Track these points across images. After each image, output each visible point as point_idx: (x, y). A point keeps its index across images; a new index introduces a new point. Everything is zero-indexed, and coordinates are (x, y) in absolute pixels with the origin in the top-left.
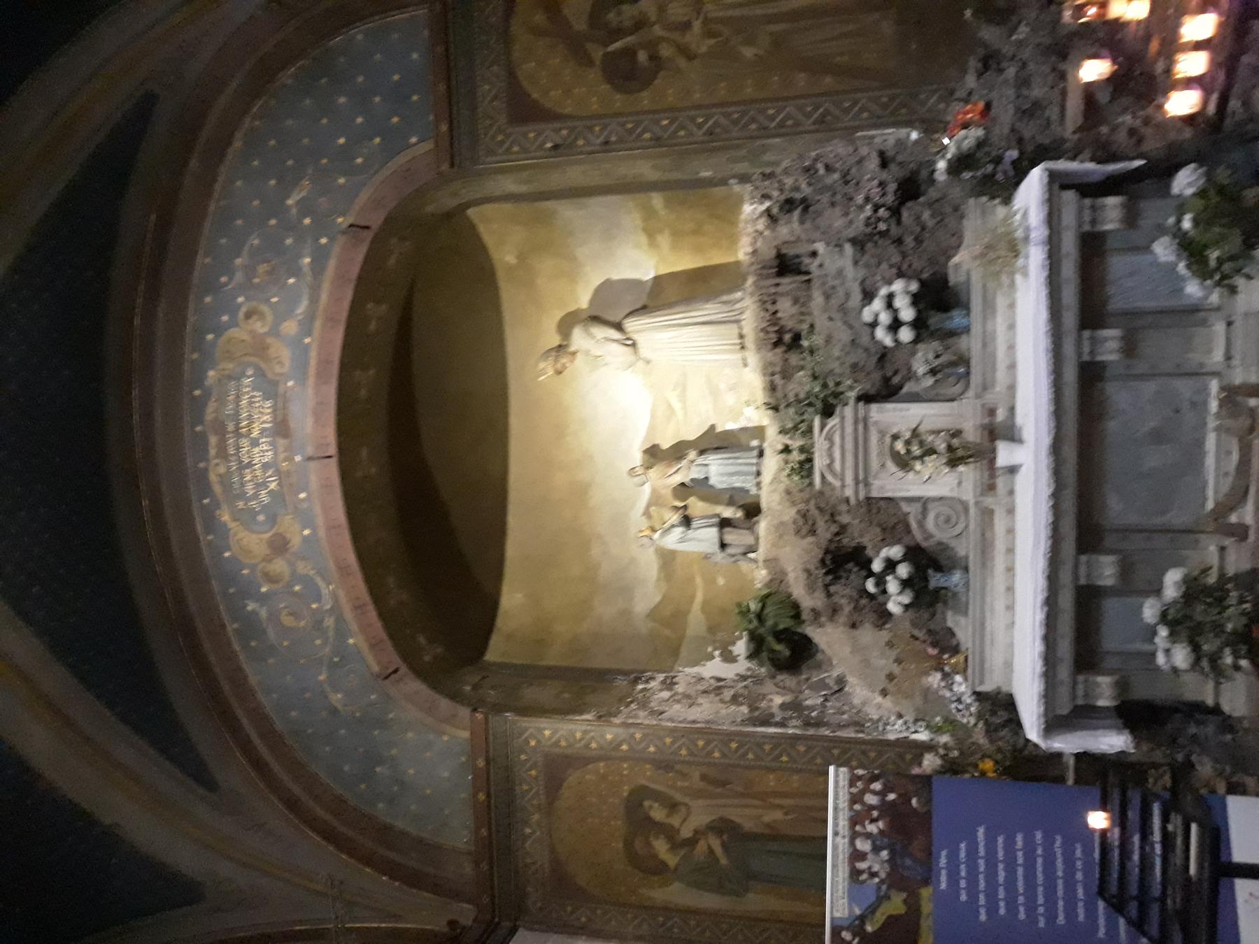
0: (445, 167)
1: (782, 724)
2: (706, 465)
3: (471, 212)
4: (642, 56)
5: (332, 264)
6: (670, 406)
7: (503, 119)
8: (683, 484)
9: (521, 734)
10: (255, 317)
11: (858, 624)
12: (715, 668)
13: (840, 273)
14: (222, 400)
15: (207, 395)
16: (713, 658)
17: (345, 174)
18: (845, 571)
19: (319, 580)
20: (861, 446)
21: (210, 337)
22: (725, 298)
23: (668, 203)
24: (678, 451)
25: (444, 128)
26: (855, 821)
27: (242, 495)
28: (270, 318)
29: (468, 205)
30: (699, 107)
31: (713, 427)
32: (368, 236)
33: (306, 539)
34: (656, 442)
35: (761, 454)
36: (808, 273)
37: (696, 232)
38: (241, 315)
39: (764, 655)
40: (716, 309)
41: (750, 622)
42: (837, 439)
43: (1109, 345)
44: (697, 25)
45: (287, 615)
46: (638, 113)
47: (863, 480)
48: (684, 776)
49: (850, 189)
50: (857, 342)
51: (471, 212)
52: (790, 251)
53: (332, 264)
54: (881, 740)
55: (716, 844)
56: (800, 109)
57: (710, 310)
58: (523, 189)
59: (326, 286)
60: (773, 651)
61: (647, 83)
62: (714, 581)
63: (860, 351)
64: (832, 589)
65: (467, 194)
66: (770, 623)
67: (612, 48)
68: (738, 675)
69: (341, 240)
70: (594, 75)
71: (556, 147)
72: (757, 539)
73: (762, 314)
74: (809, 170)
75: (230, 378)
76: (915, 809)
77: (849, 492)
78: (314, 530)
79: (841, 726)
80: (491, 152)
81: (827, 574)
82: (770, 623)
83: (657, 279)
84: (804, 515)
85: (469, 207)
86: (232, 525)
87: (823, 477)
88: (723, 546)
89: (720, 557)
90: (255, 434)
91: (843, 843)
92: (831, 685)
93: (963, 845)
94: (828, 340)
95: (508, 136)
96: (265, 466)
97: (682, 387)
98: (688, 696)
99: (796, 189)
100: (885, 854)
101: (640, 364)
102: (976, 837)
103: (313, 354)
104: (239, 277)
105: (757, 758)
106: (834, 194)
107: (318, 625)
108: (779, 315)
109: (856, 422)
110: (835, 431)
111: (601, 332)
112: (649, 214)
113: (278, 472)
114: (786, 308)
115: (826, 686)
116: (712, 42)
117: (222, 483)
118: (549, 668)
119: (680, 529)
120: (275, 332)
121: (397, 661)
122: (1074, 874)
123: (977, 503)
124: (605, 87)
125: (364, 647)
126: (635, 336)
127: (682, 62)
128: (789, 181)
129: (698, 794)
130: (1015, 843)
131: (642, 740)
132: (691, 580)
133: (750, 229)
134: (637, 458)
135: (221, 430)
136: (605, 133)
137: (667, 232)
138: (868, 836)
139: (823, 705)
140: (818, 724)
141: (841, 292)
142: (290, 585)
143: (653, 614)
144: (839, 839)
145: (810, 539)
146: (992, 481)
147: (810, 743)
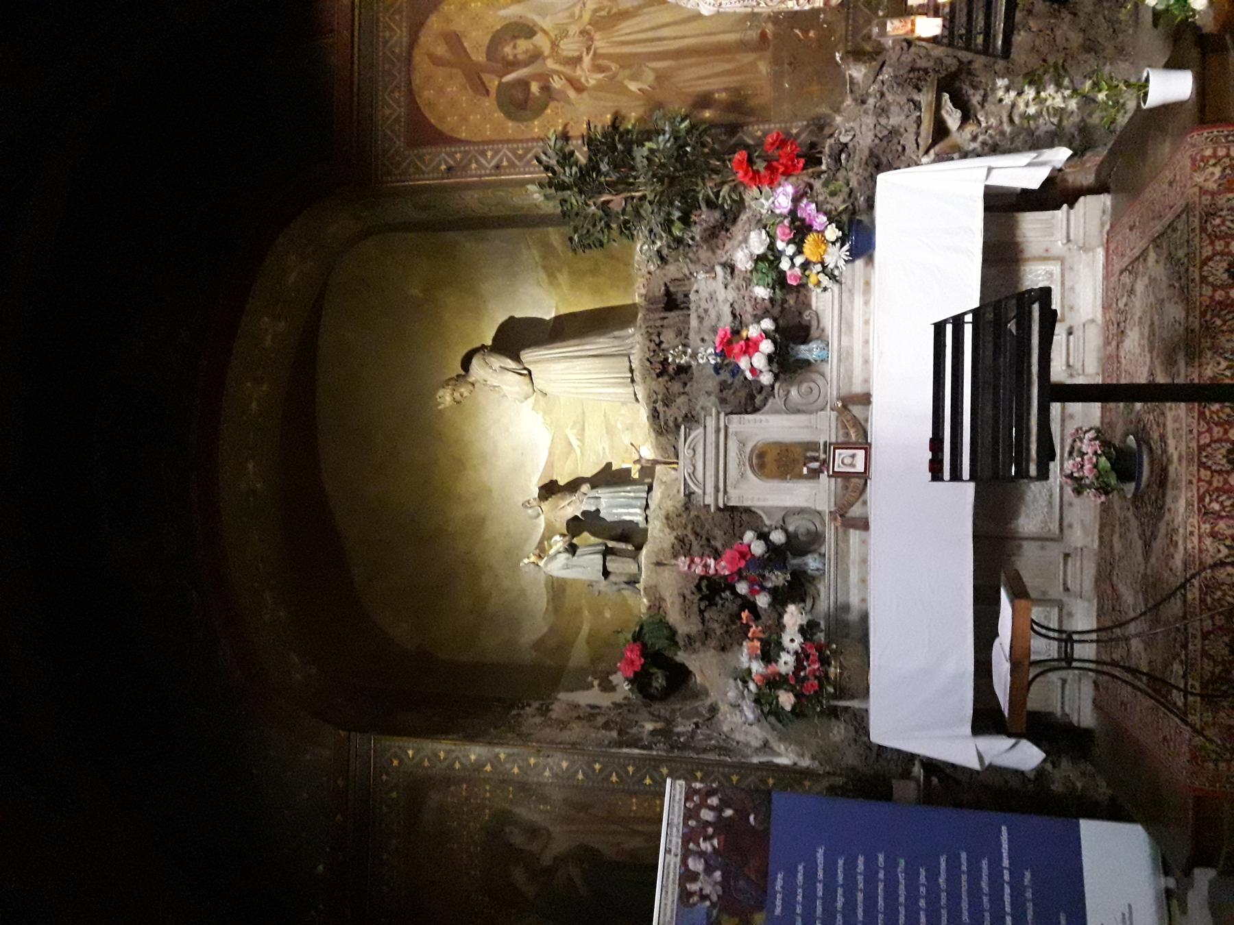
1: (649, 748)
2: (597, 498)
4: (535, 87)
8: (575, 518)
11: (728, 647)
12: (592, 696)
13: (712, 297)
16: (593, 686)
18: (722, 598)
20: (721, 454)
22: (617, 333)
24: (574, 486)
26: (688, 838)
31: (609, 465)
34: (555, 478)
35: (650, 489)
40: (605, 343)
42: (700, 450)
44: (587, 60)
46: (527, 141)
54: (743, 763)
55: (574, 871)
57: (601, 344)
61: (539, 110)
62: (601, 613)
67: (507, 79)
68: (613, 703)
70: (489, 103)
71: (449, 169)
72: (640, 568)
73: (648, 343)
76: (753, 827)
77: (709, 500)
79: (705, 751)
83: (557, 318)
84: (681, 540)
88: (606, 573)
89: (603, 584)
91: (674, 861)
93: (800, 868)
98: (562, 722)
100: (718, 875)
102: (815, 857)
108: (663, 346)
109: (718, 431)
110: (698, 442)
112: (547, 249)
115: (698, 714)
116: (600, 76)
119: (565, 555)
122: (917, 901)
124: (498, 115)
127: (572, 94)
130: (856, 867)
133: (644, 271)
134: (535, 492)
137: (565, 271)
138: (701, 854)
139: (694, 732)
140: (685, 747)
143: (539, 645)
144: (670, 857)
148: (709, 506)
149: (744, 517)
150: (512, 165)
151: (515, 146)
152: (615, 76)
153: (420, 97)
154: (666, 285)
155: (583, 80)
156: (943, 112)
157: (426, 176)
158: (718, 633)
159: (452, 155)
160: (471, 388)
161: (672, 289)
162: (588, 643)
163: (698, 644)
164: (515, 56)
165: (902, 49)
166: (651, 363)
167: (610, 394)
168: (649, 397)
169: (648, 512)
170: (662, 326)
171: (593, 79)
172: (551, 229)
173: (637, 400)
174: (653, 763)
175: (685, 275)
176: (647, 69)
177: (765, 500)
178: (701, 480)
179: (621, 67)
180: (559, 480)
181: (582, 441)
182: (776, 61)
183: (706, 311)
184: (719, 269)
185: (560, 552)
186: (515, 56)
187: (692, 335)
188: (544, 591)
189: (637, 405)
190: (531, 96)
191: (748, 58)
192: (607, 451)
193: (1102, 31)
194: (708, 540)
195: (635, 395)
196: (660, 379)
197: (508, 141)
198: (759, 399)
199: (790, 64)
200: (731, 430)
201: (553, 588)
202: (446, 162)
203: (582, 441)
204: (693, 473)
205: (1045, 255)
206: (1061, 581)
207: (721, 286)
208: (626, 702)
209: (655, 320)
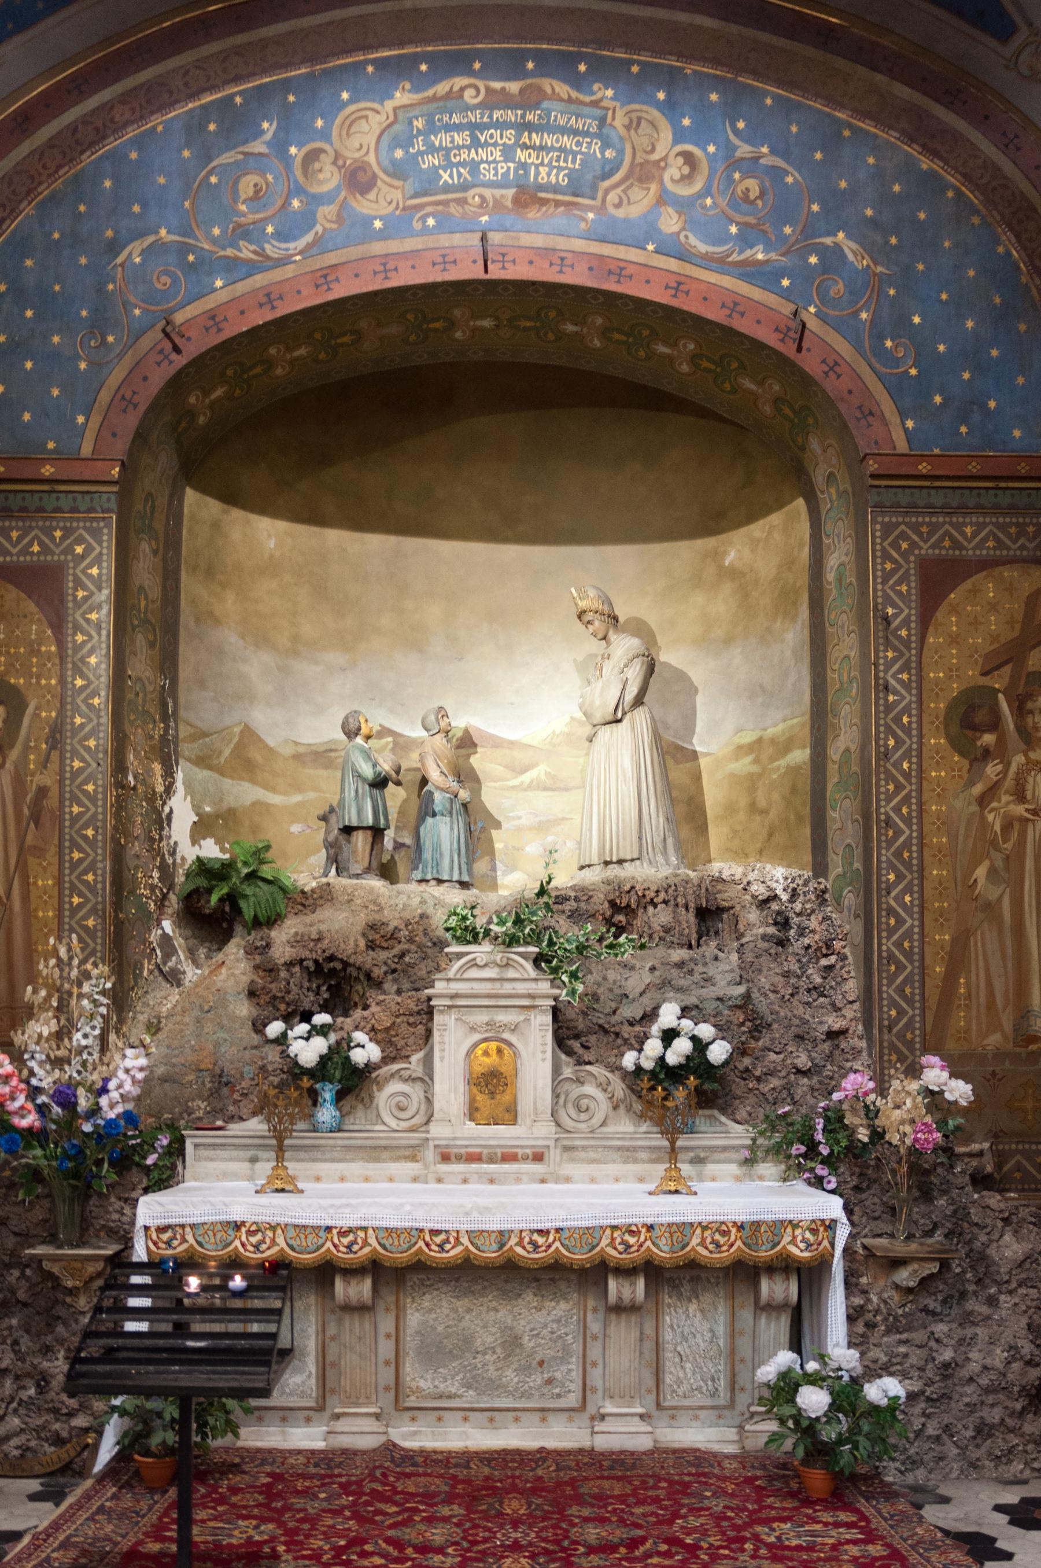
0: (872, 466)
2: (451, 813)
4: (988, 739)
5: (756, 293)
7: (925, 549)
9: (90, 531)
10: (686, 170)
15: (577, 82)
18: (318, 987)
19: (309, 238)
20: (496, 1002)
21: (661, 96)
22: (670, 841)
23: (793, 770)
24: (464, 775)
25: (924, 468)
27: (431, 128)
28: (685, 191)
30: (921, 811)
31: (498, 825)
32: (788, 349)
33: (368, 221)
34: (479, 749)
36: (699, 945)
37: (753, 808)
39: (202, 882)
40: (657, 828)
41: (246, 864)
44: (1020, 810)
45: (256, 185)
46: (920, 728)
48: (45, 764)
50: (625, 1001)
51: (800, 503)
53: (756, 293)
56: (908, 935)
57: (656, 823)
58: (830, 576)
59: (727, 282)
60: (209, 891)
61: (959, 745)
63: (614, 1005)
64: (297, 969)
65: (830, 498)
66: (248, 891)
68: (176, 843)
69: (787, 309)
70: (972, 674)
71: (887, 620)
72: (357, 876)
73: (654, 888)
75: (602, 122)
77: (440, 987)
78: (383, 236)
81: (316, 961)
82: (248, 891)
83: (694, 755)
85: (806, 500)
86: (389, 105)
87: (460, 955)
88: (348, 830)
90: (521, 155)
92: (170, 964)
95: (905, 555)
97: (552, 786)
101: (588, 730)
104: (744, 150)
105: (75, 865)
106: (798, 977)
107: (244, 233)
108: (651, 909)
111: (635, 674)
113: (464, 187)
114: (660, 917)
116: (997, 828)
117: (449, 95)
118: (177, 581)
120: (663, 199)
121: (192, 350)
123: (427, 1139)
125: (209, 303)
126: (625, 721)
127: (978, 789)
128: (814, 923)
129: (19, 782)
131: (90, 706)
132: (298, 787)
134: (459, 722)
135: (529, 100)
136: (899, 687)
137: (755, 769)
142: (300, 191)
143: (249, 734)
145: (362, 943)
146: (453, 1158)
147: (99, 934)
148: (433, 987)
149: (421, 1029)
150: (889, 708)
151: (914, 712)
152: (997, 849)
153: (986, 577)
154: (732, 908)
155: (994, 804)
156: (916, 1266)
157: (880, 587)
158: (273, 986)
159: (906, 623)
160: (600, 636)
161: (725, 916)
162: (254, 804)
163: (258, 959)
164: (1031, 712)
165: (1001, 1211)
166: (629, 892)
167: (591, 831)
168: (583, 889)
169: (433, 883)
170: (677, 905)
172: (808, 751)
173: (582, 868)
174: (100, 907)
175: (742, 935)
176: (999, 892)
177: (442, 1059)
178: (465, 976)
179: (1008, 857)
180: (477, 756)
181: (530, 787)
182: (999, 1055)
183: (691, 972)
184: (741, 990)
185: (374, 766)
186: (1031, 712)
187: (661, 952)
188: (325, 739)
189: (576, 866)
190: (978, 734)
191: (1007, 1022)
192: (516, 823)
193: (999, 1443)
194: (394, 971)
195: (589, 866)
196: (606, 905)
199: (994, 1074)
200: (532, 1014)
201: (331, 750)
202: (896, 616)
203: (530, 787)
204: (476, 965)
205: (737, 1387)
206: (347, 1410)
207: (721, 993)
208: (179, 861)
209: (684, 895)
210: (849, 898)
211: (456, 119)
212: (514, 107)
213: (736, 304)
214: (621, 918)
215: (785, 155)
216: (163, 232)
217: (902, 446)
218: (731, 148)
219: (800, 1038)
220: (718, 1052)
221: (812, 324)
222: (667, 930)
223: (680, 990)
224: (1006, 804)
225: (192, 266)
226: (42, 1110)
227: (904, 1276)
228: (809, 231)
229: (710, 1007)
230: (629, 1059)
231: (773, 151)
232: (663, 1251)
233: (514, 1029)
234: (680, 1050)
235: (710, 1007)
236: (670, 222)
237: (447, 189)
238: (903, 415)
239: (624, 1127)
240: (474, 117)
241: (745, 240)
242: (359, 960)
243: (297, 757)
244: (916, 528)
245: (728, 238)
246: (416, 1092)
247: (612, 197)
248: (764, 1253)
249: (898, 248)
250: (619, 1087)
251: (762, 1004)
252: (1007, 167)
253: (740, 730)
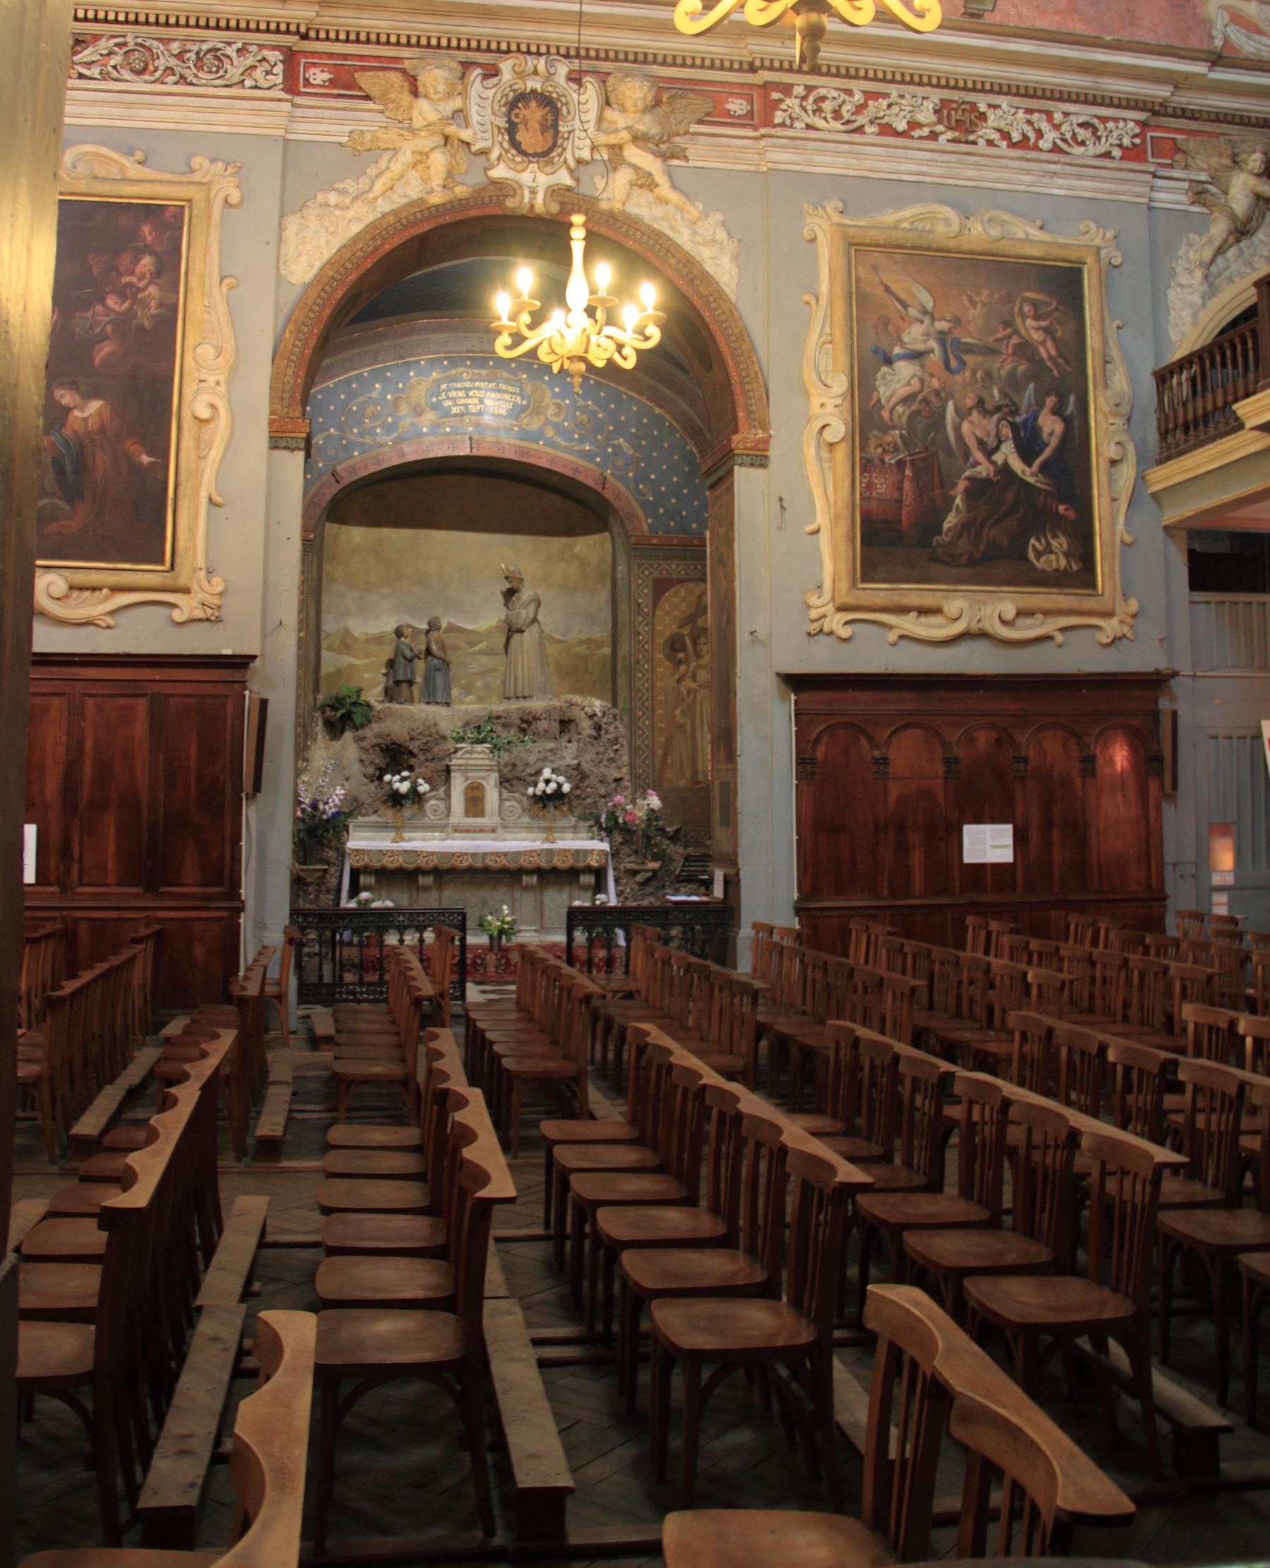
3: (607, 534)
4: (681, 655)
6: (476, 644)
7: (656, 574)
13: (563, 758)
14: (507, 382)
17: (635, 477)
20: (478, 768)
25: (655, 541)
28: (556, 420)
29: (611, 534)
32: (599, 488)
38: (558, 401)
43: (426, 964)
44: (693, 685)
47: (465, 769)
49: (605, 763)
52: (572, 727)
56: (647, 738)
58: (619, 575)
59: (573, 458)
61: (668, 658)
69: (598, 471)
71: (639, 605)
74: (616, 741)
77: (454, 762)
80: (640, 566)
86: (430, 378)
94: (528, 751)
96: (466, 406)
99: (607, 732)
103: (534, 446)
113: (462, 415)
121: (345, 482)
127: (677, 676)
133: (586, 703)
141: (552, 758)
143: (347, 632)
145: (408, 737)
150: (639, 642)
159: (647, 606)
171: (683, 690)
191: (688, 774)
197: (653, 638)
198: (507, 784)
210: (626, 719)
211: (459, 385)
212: (484, 381)
213: (577, 469)
214: (524, 725)
215: (599, 406)
216: (332, 430)
217: (646, 530)
218: (576, 402)
219: (601, 782)
220: (566, 788)
221: (609, 478)
222: (546, 731)
223: (551, 761)
224: (688, 684)
225: (345, 446)
226: (303, 811)
227: (639, 878)
228: (609, 437)
229: (563, 769)
230: (530, 790)
231: (594, 403)
232: (543, 863)
233: (483, 778)
234: (552, 787)
235: (563, 769)
236: (550, 432)
237: (455, 415)
238: (647, 517)
239: (526, 820)
240: (467, 385)
241: (582, 440)
242: (406, 744)
243: (367, 641)
244: (651, 565)
245: (573, 440)
246: (442, 804)
247: (525, 422)
248: (581, 864)
249: (645, 446)
250: (526, 803)
251: (586, 767)
252: (691, 413)
253: (580, 632)
